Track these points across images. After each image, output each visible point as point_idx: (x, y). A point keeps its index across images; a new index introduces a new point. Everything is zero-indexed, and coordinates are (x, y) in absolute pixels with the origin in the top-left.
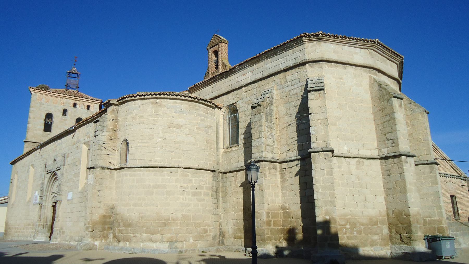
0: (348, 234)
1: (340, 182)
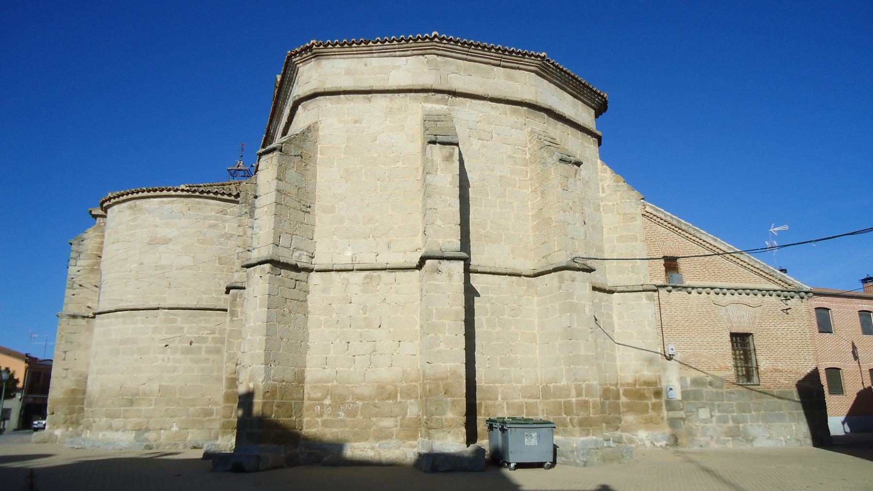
0: (325, 417)
1: (322, 318)
